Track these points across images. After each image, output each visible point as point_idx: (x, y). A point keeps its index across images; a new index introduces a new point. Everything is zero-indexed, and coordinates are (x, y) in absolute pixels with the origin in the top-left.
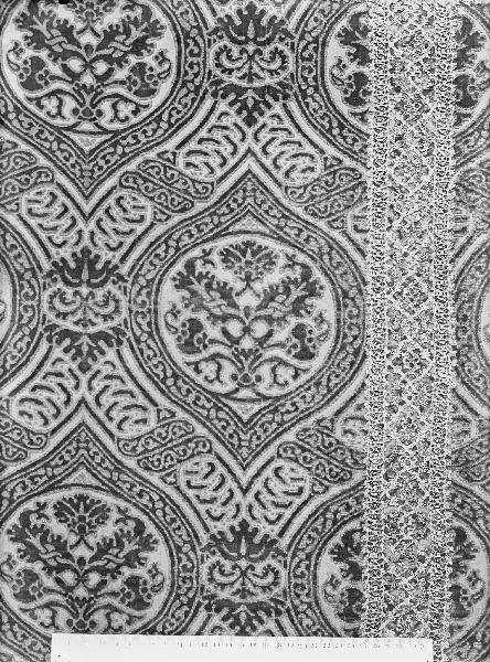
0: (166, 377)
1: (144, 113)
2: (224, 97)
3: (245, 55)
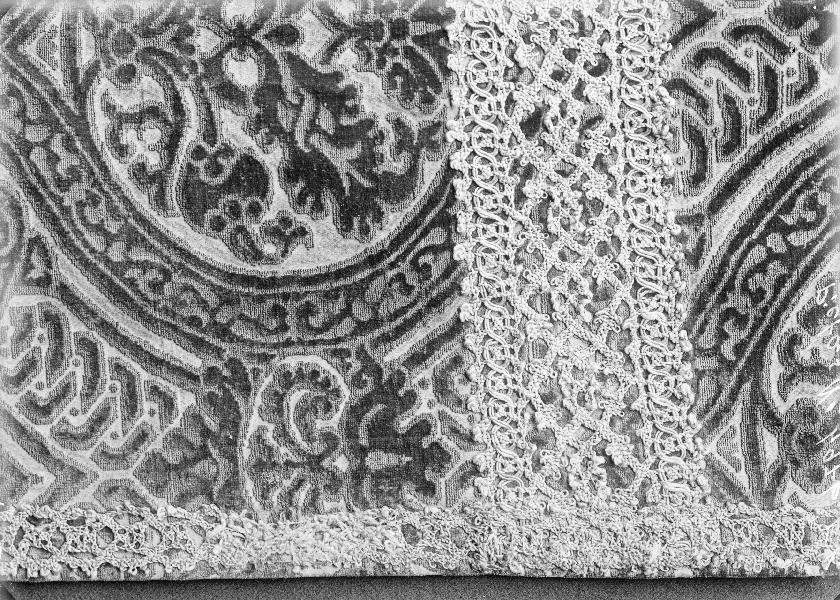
0: (786, 230)
1: (142, 200)
2: (211, 399)
3: (318, 448)
